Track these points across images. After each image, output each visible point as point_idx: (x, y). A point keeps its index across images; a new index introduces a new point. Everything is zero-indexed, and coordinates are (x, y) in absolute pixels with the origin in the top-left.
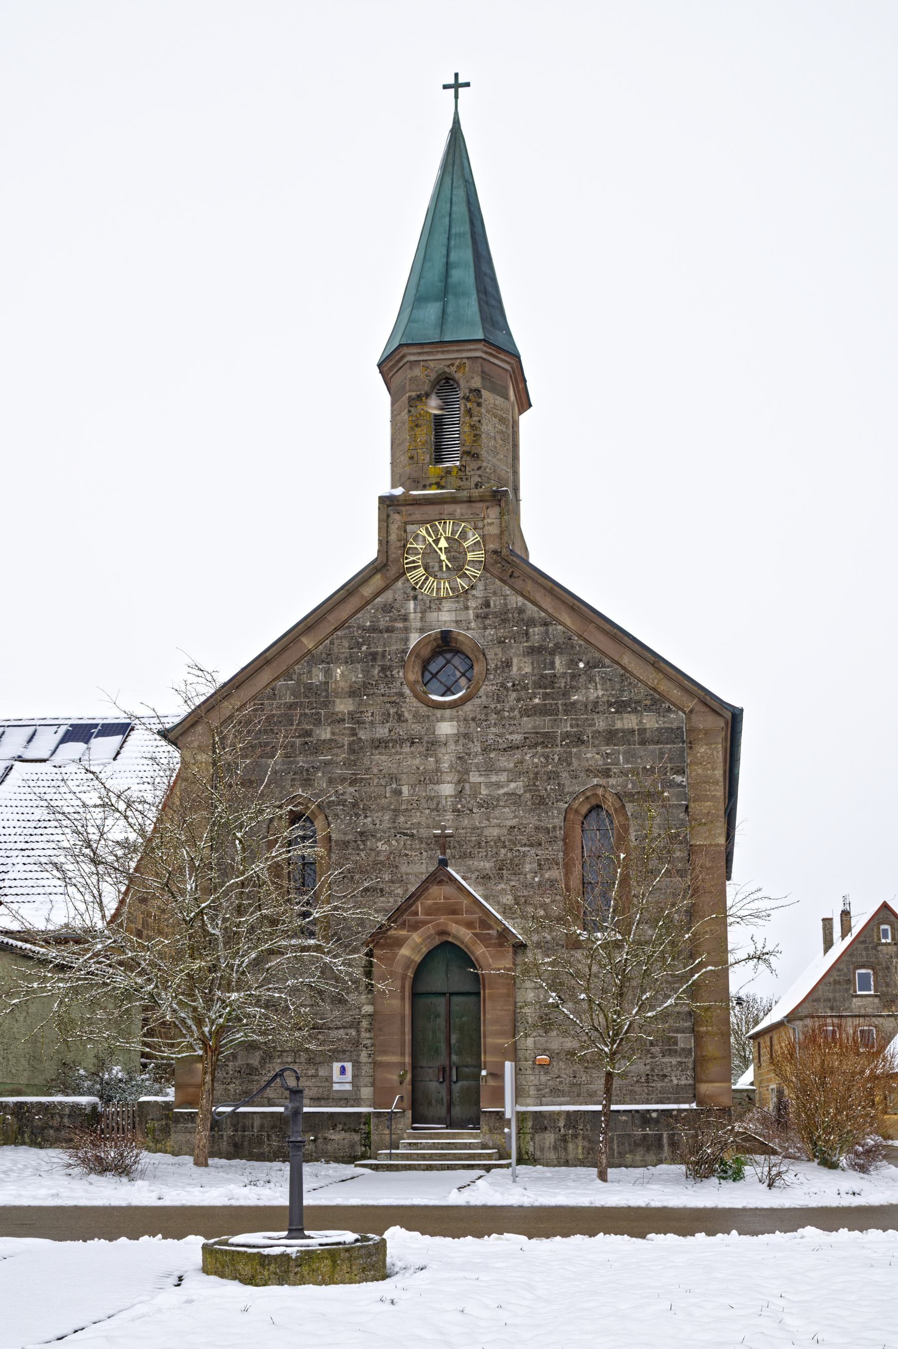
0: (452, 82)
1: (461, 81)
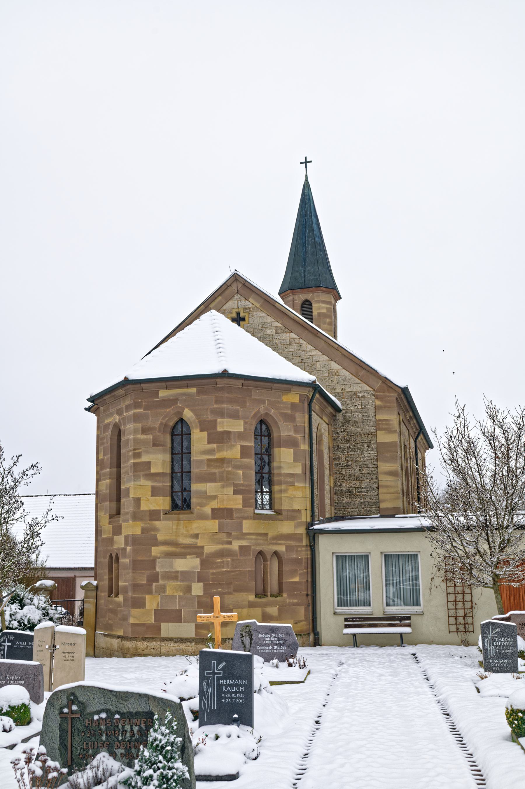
0: (304, 161)
1: (308, 160)
